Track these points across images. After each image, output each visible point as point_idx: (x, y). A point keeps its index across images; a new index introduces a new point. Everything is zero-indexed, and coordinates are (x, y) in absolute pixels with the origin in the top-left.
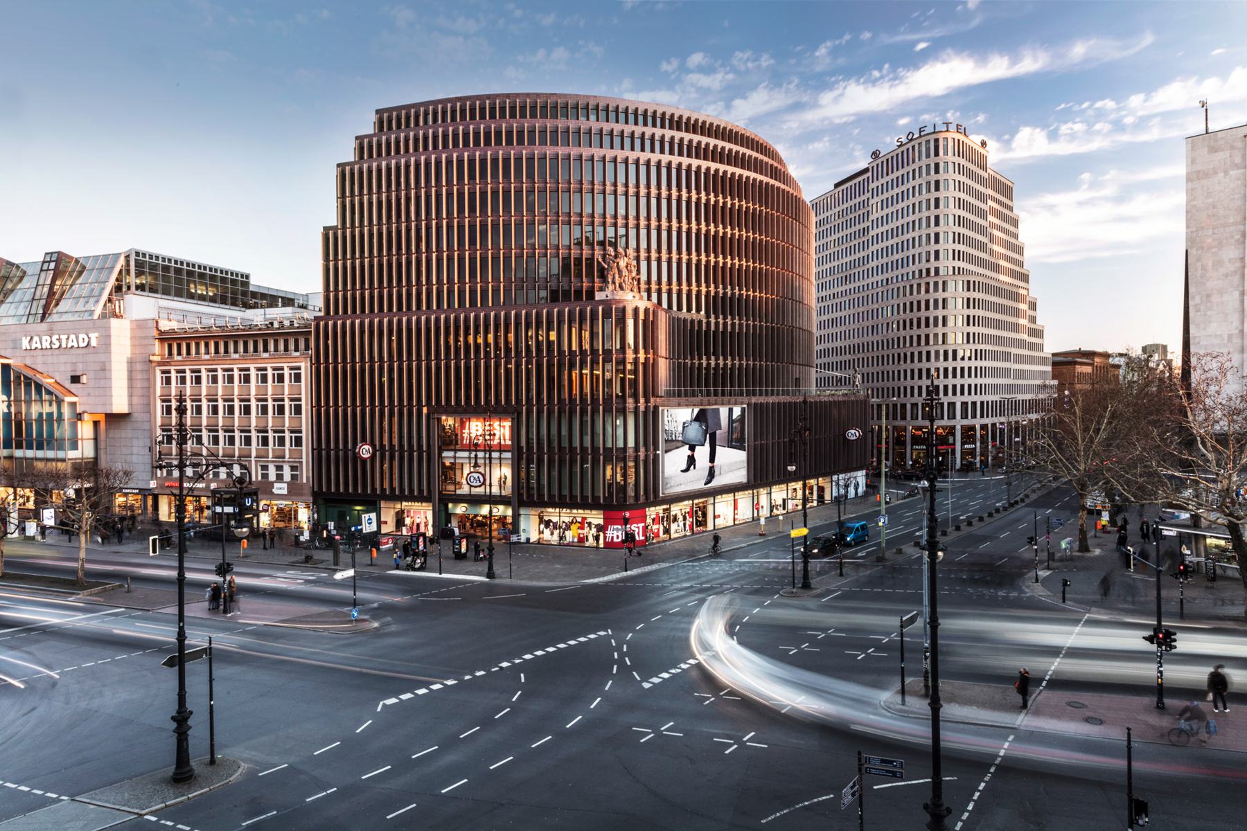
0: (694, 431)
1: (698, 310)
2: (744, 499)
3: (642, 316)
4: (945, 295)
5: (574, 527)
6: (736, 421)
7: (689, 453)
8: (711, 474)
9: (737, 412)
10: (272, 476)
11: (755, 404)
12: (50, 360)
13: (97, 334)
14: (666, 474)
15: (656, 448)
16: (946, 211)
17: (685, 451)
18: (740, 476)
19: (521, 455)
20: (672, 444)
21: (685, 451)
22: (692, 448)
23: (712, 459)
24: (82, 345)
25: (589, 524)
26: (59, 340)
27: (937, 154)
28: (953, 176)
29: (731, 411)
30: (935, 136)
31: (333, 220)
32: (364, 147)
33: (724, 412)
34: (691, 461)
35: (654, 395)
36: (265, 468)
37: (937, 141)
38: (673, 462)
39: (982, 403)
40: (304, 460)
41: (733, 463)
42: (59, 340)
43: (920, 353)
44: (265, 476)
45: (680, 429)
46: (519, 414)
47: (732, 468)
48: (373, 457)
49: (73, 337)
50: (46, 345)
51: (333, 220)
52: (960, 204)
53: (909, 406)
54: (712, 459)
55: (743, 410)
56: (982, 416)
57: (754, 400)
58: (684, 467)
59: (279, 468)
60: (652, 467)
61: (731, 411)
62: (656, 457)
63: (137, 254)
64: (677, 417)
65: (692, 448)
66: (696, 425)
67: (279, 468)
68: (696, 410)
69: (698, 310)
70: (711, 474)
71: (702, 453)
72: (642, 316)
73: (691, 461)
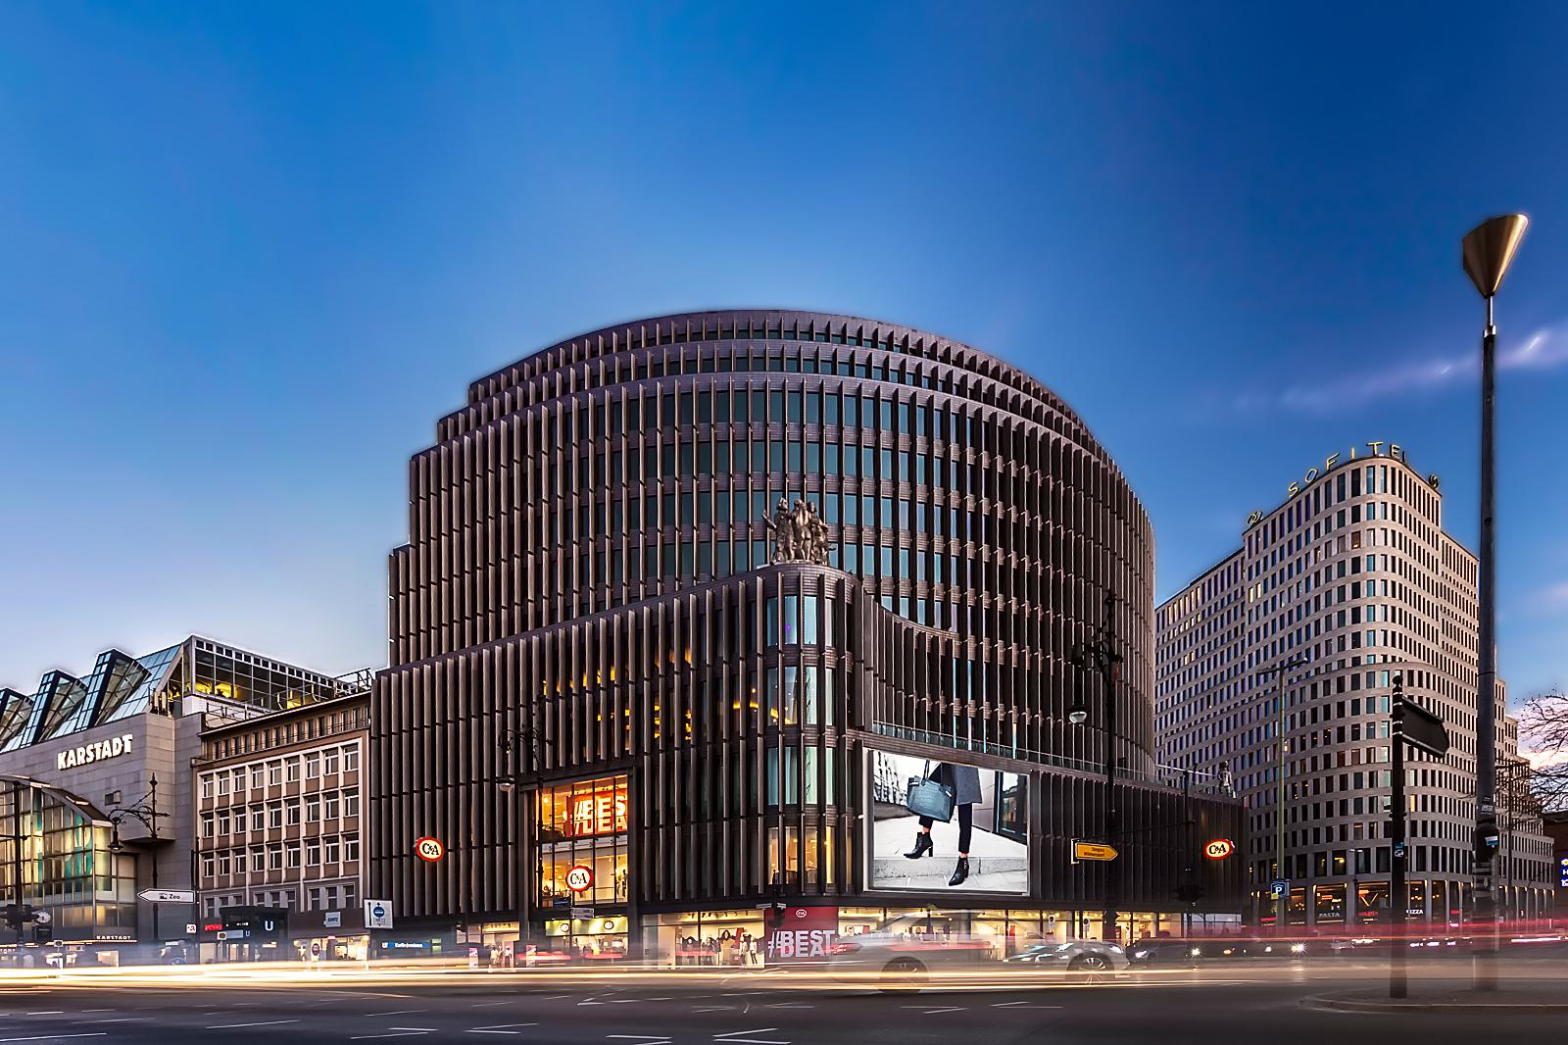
0: (930, 796)
1: (946, 626)
2: (1024, 924)
3: (829, 593)
4: (1372, 693)
5: (725, 946)
6: (1009, 794)
7: (921, 829)
8: (962, 871)
9: (1010, 781)
10: (324, 905)
11: (1046, 776)
12: (85, 778)
13: (130, 737)
14: (879, 852)
15: (857, 809)
16: (1371, 575)
17: (912, 826)
18: (1017, 882)
19: (641, 836)
20: (888, 809)
21: (912, 826)
22: (927, 822)
23: (964, 844)
24: (116, 752)
25: (748, 939)
26: (94, 750)
27: (1356, 492)
28: (1381, 573)
29: (999, 779)
30: (1354, 466)
31: (403, 538)
32: (448, 427)
33: (986, 776)
34: (924, 843)
35: (852, 726)
36: (316, 893)
37: (1356, 473)
38: (892, 839)
39: (1435, 850)
40: (361, 876)
41: (1002, 861)
42: (94, 750)
43: (1329, 780)
44: (316, 904)
45: (904, 787)
46: (640, 772)
47: (1002, 866)
48: (445, 856)
49: (107, 744)
50: (81, 760)
51: (403, 538)
52: (1394, 564)
53: (1311, 858)
54: (964, 844)
55: (1022, 781)
56: (1435, 868)
57: (1042, 769)
58: (911, 849)
59: (332, 891)
60: (852, 839)
61: (999, 779)
62: (857, 826)
63: (200, 643)
64: (900, 769)
65: (927, 822)
66: (934, 787)
67: (332, 891)
68: (934, 765)
69: (946, 626)
70: (962, 871)
71: (946, 834)
72: (829, 593)
73: (924, 843)
